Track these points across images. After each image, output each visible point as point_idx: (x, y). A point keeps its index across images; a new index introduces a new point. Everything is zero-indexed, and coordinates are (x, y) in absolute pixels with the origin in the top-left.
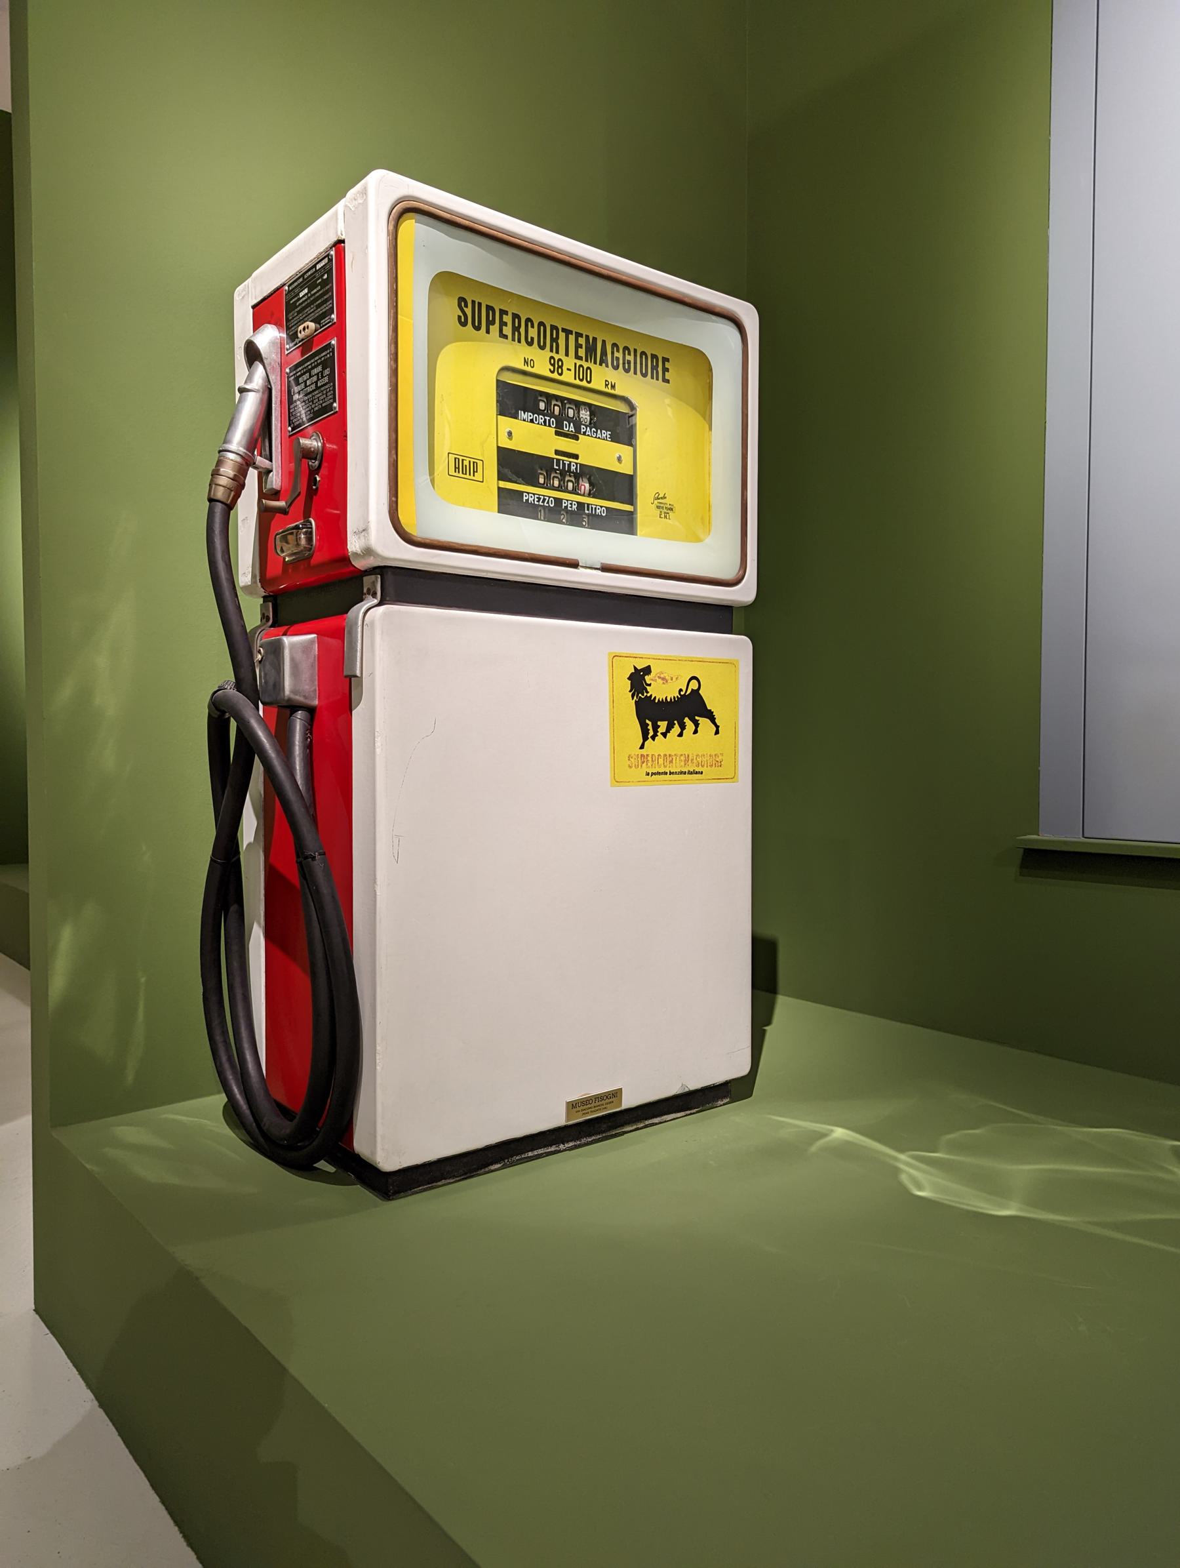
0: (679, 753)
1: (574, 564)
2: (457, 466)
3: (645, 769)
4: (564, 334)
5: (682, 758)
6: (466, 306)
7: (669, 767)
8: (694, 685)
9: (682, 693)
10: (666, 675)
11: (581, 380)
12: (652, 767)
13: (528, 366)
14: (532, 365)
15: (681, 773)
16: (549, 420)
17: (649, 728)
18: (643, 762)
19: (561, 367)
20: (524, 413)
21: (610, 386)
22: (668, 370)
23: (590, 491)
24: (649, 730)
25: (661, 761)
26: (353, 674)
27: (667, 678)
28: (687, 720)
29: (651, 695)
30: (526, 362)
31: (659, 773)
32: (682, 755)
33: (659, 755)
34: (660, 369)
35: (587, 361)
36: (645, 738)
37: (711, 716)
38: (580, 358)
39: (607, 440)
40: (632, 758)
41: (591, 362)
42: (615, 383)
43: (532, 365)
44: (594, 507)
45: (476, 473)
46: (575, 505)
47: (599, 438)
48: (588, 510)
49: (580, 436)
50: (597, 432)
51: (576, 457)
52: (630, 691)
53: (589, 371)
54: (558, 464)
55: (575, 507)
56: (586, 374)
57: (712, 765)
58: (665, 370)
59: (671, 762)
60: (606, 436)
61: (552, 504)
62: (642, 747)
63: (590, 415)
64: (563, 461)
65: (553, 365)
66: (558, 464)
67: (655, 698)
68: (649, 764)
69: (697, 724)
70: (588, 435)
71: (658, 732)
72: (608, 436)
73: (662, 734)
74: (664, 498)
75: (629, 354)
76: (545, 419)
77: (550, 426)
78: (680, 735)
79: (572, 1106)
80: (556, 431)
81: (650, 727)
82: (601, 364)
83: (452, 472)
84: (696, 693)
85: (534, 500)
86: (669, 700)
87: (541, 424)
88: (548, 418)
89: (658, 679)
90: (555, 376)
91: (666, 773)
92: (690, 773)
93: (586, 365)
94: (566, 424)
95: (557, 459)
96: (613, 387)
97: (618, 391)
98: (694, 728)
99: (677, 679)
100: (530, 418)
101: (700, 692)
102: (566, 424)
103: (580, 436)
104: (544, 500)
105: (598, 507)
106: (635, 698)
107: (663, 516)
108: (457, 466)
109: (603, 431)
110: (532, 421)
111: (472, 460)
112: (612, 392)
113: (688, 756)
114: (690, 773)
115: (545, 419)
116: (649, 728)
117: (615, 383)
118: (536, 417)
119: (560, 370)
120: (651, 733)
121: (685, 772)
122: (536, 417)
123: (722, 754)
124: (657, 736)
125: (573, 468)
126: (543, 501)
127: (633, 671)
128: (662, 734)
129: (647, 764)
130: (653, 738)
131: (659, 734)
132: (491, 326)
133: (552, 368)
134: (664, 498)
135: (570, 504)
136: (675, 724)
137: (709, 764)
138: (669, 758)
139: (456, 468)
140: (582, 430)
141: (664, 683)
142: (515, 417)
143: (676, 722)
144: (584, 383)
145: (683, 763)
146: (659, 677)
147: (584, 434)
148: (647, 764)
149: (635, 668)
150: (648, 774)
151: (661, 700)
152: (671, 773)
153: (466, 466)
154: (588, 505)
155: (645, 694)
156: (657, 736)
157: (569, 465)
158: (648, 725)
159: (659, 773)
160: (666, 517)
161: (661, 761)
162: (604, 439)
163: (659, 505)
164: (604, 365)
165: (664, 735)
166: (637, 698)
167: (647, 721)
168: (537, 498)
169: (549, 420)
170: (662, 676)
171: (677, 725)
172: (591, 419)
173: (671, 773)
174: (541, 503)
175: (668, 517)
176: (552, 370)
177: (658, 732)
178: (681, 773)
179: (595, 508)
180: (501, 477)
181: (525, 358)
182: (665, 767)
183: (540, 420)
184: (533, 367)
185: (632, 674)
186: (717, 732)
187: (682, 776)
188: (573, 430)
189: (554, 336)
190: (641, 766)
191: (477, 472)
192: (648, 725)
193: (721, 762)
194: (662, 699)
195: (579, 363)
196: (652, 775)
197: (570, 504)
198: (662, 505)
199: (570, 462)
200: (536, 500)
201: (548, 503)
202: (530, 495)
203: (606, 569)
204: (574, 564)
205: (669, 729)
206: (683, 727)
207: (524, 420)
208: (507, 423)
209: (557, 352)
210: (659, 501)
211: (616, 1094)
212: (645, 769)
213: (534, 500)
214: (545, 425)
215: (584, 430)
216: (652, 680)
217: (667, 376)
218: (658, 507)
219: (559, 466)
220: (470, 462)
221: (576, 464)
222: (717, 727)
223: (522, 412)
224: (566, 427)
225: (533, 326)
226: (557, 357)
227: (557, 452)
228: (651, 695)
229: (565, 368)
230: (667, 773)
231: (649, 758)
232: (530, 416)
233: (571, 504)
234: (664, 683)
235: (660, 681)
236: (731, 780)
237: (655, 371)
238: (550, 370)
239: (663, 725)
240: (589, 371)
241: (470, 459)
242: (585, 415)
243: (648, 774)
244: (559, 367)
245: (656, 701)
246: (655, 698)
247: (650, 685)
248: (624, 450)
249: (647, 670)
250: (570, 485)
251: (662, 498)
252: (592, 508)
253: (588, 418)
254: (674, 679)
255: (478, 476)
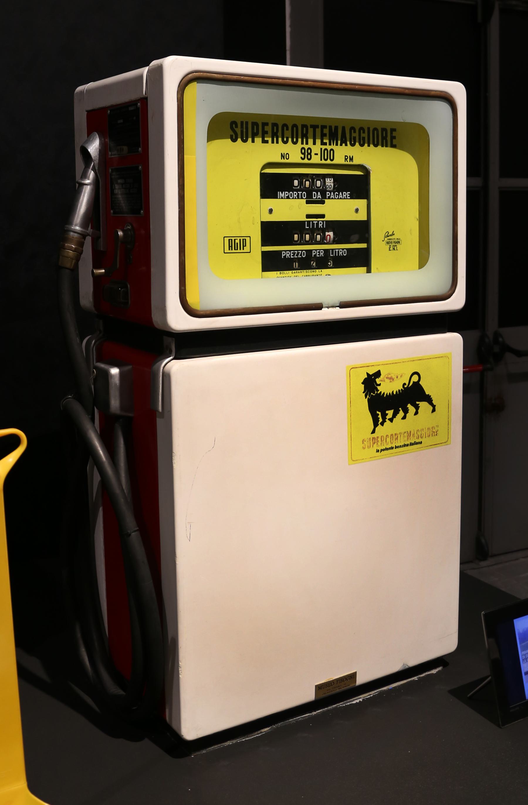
0: (403, 431)
1: (318, 307)
2: (231, 245)
3: (376, 447)
4: (312, 129)
5: (406, 435)
6: (236, 127)
7: (395, 443)
8: (415, 378)
9: (405, 386)
10: (392, 375)
11: (326, 160)
12: (381, 446)
13: (284, 159)
14: (287, 158)
15: (405, 445)
16: (301, 194)
17: (379, 417)
18: (374, 443)
19: (310, 154)
20: (282, 193)
21: (348, 160)
22: (394, 138)
23: (334, 238)
24: (379, 418)
25: (388, 440)
26: (317, 137)
27: (393, 377)
28: (409, 406)
29: (381, 392)
30: (283, 156)
31: (387, 449)
32: (405, 432)
33: (387, 436)
34: (389, 138)
35: (330, 144)
36: (376, 424)
37: (428, 399)
38: (325, 144)
39: (347, 199)
40: (365, 441)
41: (333, 145)
42: (353, 156)
43: (287, 158)
44: (337, 250)
45: (244, 247)
46: (322, 252)
47: (341, 198)
48: (332, 254)
49: (326, 200)
50: (339, 195)
51: (323, 216)
52: (364, 393)
53: (332, 152)
54: (309, 225)
55: (322, 254)
56: (330, 154)
57: (430, 436)
58: (393, 138)
59: (397, 439)
60: (346, 196)
61: (304, 255)
62: (373, 432)
63: (334, 182)
64: (312, 221)
65: (304, 154)
66: (309, 225)
67: (384, 393)
68: (379, 444)
69: (417, 407)
70: (332, 198)
71: (386, 418)
72: (348, 195)
73: (389, 419)
74: (393, 234)
75: (364, 132)
76: (298, 194)
77: (302, 198)
78: (404, 418)
79: (319, 688)
80: (306, 201)
81: (380, 416)
82: (341, 145)
83: (227, 250)
84: (417, 385)
85: (290, 256)
86: (395, 393)
87: (295, 198)
88: (300, 193)
89: (386, 379)
90: (306, 161)
91: (392, 448)
92: (412, 444)
93: (329, 147)
94: (315, 194)
95: (308, 221)
96: (351, 159)
97: (356, 162)
98: (415, 410)
99: (401, 376)
100: (286, 195)
101: (420, 383)
102: (315, 194)
103: (326, 200)
104: (298, 253)
105: (340, 250)
106: (368, 397)
107: (392, 249)
108: (231, 245)
109: (344, 193)
110: (288, 198)
111: (242, 238)
112: (351, 163)
113: (410, 432)
114: (412, 444)
115: (298, 194)
116: (379, 417)
117: (353, 156)
118: (291, 194)
119: (309, 156)
120: (381, 420)
121: (408, 444)
122: (291, 194)
123: (438, 426)
124: (386, 421)
125: (320, 225)
126: (297, 255)
127: (366, 377)
128: (389, 419)
129: (377, 444)
130: (382, 424)
131: (387, 420)
132: (265, 127)
133: (303, 156)
134: (393, 234)
135: (318, 252)
136: (400, 410)
137: (427, 436)
138: (394, 437)
139: (230, 247)
140: (327, 196)
141: (391, 382)
142: (276, 197)
143: (400, 409)
144: (329, 162)
145: (406, 438)
146: (387, 378)
147: (329, 198)
148: (377, 444)
149: (367, 374)
150: (378, 451)
151: (388, 394)
152: (396, 447)
153: (237, 243)
154: (333, 250)
155: (376, 392)
156: (386, 421)
157: (317, 224)
158: (378, 415)
159: (387, 449)
160: (394, 249)
161: (388, 440)
162: (345, 199)
163: (389, 241)
164: (344, 144)
165: (391, 420)
166: (369, 396)
167: (378, 412)
168: (292, 253)
169: (301, 194)
170: (389, 376)
171: (401, 411)
172: (334, 185)
173: (396, 447)
174: (295, 257)
175: (396, 249)
176: (303, 157)
177: (386, 418)
178: (405, 445)
179: (338, 251)
180: (264, 243)
181: (282, 154)
182: (392, 443)
183: (294, 195)
184: (288, 159)
185: (365, 379)
186: (434, 410)
187: (406, 448)
188: (320, 197)
189: (305, 132)
190: (373, 446)
191: (245, 246)
192: (378, 415)
193: (436, 432)
194: (390, 393)
195: (324, 147)
196: (381, 451)
197: (318, 252)
198: (391, 241)
199: (318, 221)
200: (292, 254)
201: (301, 255)
202: (287, 252)
203: (344, 305)
204: (318, 307)
205: (394, 415)
206: (406, 411)
207: (282, 198)
208: (270, 203)
209: (307, 143)
210: (389, 238)
211: (353, 676)
212: (376, 447)
213: (290, 256)
214: (298, 198)
215: (329, 195)
216: (381, 381)
217: (395, 142)
218: (388, 243)
219: (310, 227)
220: (240, 240)
221: (323, 221)
222: (434, 406)
223: (280, 192)
224: (315, 197)
225: (287, 129)
226: (306, 147)
227: (308, 216)
228: (381, 392)
229: (313, 154)
230: (393, 447)
231: (379, 439)
232: (287, 194)
233: (319, 252)
234: (391, 382)
235: (387, 381)
236: (445, 444)
237: (384, 141)
238: (301, 158)
239: (390, 413)
240: (332, 152)
241: (240, 238)
242: (329, 182)
243: (378, 451)
244: (308, 154)
245: (385, 396)
246: (384, 393)
247: (380, 385)
248: (361, 203)
249: (378, 374)
250: (319, 237)
251: (391, 235)
252: (336, 252)
253: (332, 185)
254: (399, 377)
255: (247, 249)
